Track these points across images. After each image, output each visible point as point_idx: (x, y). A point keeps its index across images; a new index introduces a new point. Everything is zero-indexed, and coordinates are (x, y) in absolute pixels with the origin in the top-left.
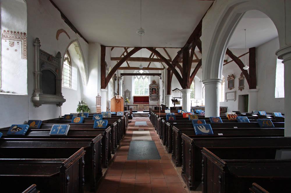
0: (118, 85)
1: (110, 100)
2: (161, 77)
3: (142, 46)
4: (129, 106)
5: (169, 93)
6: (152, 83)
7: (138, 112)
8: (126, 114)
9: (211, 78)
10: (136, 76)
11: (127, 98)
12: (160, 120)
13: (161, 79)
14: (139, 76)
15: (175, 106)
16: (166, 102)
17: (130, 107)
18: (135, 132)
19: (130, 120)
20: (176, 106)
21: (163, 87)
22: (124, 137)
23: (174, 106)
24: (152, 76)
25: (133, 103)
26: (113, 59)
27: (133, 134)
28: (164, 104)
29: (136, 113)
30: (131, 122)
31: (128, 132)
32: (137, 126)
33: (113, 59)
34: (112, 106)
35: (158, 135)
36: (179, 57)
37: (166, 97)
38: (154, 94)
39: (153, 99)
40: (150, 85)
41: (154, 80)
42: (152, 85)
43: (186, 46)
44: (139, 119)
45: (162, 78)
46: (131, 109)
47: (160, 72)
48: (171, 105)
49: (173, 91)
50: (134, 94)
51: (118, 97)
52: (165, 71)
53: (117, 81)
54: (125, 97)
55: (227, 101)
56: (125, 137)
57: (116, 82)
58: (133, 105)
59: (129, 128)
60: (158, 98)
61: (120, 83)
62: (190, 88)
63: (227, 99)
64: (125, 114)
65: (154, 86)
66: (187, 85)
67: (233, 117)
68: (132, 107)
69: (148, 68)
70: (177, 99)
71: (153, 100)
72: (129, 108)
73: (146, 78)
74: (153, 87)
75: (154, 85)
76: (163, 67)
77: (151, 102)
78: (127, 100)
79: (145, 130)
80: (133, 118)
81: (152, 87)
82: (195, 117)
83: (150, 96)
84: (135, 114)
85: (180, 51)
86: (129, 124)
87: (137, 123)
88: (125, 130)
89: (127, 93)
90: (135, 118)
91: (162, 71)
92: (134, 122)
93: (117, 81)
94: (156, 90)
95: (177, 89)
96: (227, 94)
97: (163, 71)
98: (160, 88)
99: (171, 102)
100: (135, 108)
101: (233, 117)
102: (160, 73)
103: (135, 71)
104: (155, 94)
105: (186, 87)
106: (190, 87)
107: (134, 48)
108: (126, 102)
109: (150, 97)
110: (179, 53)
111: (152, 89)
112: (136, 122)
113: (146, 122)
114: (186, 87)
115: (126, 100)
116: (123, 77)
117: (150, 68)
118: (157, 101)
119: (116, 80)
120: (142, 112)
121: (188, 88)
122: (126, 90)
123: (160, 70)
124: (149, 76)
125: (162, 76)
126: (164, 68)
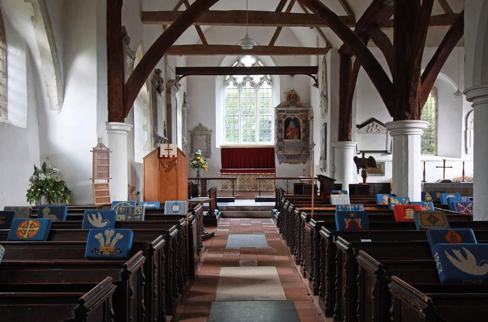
0: (169, 107)
1: (139, 159)
2: (316, 81)
4: (204, 180)
5: (344, 135)
6: (284, 100)
7: (238, 203)
8: (197, 209)
10: (228, 77)
11: (199, 152)
13: (316, 85)
14: (240, 78)
16: (333, 166)
17: (210, 185)
18: (225, 272)
19: (208, 231)
20: (371, 179)
22: (190, 285)
27: (218, 277)
28: (328, 174)
29: (230, 204)
30: (212, 236)
31: (202, 271)
33: (148, 17)
35: (306, 282)
37: (333, 149)
38: (292, 141)
40: (278, 106)
41: (292, 90)
42: (285, 106)
46: (213, 192)
47: (313, 61)
48: (353, 176)
49: (359, 127)
51: (169, 150)
52: (332, 61)
53: (163, 93)
56: (192, 289)
58: (219, 176)
59: (205, 255)
60: (306, 153)
68: (218, 185)
69: (271, 50)
71: (289, 159)
72: (204, 188)
74: (289, 116)
75: (292, 108)
76: (323, 45)
77: (282, 168)
78: (198, 160)
79: (261, 264)
80: (221, 222)
81: (285, 116)
83: (277, 145)
84: (228, 208)
86: (204, 243)
87: (235, 240)
88: (191, 264)
91: (321, 57)
92: (225, 237)
93: (163, 93)
94: (298, 125)
95: (372, 120)
97: (325, 59)
98: (312, 118)
100: (226, 187)
102: (313, 64)
103: (227, 61)
105: (407, 114)
106: (420, 114)
108: (195, 166)
109: (280, 149)
111: (284, 120)
112: (229, 236)
113: (263, 236)
114: (407, 114)
115: (195, 162)
116: (183, 81)
118: (304, 163)
119: (159, 90)
120: (250, 203)
121: (413, 118)
122: (195, 124)
123: (313, 54)
124: (277, 78)
125: (320, 75)
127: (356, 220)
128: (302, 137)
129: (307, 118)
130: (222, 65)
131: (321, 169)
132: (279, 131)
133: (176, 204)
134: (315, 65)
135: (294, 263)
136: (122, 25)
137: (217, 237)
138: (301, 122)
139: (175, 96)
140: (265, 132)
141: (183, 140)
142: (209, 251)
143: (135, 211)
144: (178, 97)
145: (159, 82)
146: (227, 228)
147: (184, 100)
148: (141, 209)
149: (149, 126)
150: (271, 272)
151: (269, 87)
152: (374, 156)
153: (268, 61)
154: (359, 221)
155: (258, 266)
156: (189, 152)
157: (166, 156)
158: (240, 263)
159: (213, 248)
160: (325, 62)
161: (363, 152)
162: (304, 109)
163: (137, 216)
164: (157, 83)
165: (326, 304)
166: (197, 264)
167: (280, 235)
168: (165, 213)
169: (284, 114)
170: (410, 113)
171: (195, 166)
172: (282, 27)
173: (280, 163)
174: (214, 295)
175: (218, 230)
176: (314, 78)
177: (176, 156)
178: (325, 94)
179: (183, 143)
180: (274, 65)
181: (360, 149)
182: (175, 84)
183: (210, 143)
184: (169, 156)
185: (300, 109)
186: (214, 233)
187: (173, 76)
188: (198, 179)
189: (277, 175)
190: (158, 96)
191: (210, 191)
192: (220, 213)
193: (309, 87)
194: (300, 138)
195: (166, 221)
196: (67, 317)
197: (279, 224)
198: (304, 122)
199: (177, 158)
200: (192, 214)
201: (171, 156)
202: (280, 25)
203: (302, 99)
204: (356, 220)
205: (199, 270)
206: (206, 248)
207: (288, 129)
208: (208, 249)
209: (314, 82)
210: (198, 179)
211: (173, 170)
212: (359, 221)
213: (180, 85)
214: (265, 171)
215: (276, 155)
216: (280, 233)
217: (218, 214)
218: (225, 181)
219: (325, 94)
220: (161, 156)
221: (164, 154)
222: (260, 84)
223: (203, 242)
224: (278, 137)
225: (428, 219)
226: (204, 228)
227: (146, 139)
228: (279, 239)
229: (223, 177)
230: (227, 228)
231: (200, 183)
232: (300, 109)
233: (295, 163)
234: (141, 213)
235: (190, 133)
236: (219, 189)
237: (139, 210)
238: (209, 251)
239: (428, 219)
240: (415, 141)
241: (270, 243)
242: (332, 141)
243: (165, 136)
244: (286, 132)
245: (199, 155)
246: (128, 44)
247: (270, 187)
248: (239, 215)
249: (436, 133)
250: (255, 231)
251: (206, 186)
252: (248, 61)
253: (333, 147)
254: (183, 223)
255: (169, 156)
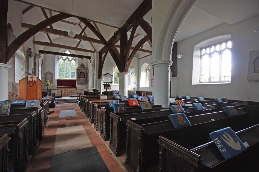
0: (35, 63)
1: (17, 81)
2: (91, 61)
3: (73, 14)
4: (50, 90)
5: (100, 76)
6: (80, 66)
7: (63, 98)
8: (45, 104)
9: (163, 59)
10: (60, 56)
11: (48, 81)
12: (87, 102)
13: (91, 62)
14: (64, 57)
15: (106, 90)
17: (52, 92)
18: (59, 131)
19: (51, 110)
20: (108, 90)
21: (93, 71)
22: (39, 145)
23: (106, 91)
24: (81, 58)
25: (57, 87)
26: (24, 25)
27: (56, 135)
29: (60, 98)
30: (53, 112)
31: (47, 133)
32: (62, 118)
33: (24, 25)
34: (22, 91)
35: (98, 133)
36: (115, 39)
37: (96, 81)
38: (82, 78)
39: (81, 83)
40: (78, 68)
41: (82, 63)
42: (80, 68)
43: (125, 25)
44: (65, 107)
45: (92, 61)
46: (54, 95)
47: (89, 54)
48: (103, 90)
49: (104, 75)
50: (57, 77)
51: (32, 78)
53: (32, 58)
54: (45, 80)
55: (151, 87)
56: (41, 147)
57: (31, 59)
58: (56, 89)
59: (49, 123)
60: (86, 82)
61: (37, 62)
62: (127, 72)
63: (152, 84)
64: (42, 105)
65: (82, 70)
66: (125, 69)
67: (182, 104)
68: (56, 92)
69: (76, 49)
70: (109, 83)
71: (81, 84)
72: (50, 93)
73: (73, 60)
74: (81, 71)
75: (82, 69)
76: (93, 50)
78: (47, 83)
79: (76, 124)
80: (57, 105)
81: (80, 71)
82: (148, 106)
83: (77, 80)
84: (60, 100)
85: (116, 32)
86: (49, 116)
87: (63, 114)
88: (40, 129)
89: (48, 75)
90: (59, 105)
91: (93, 54)
92: (58, 112)
93: (32, 58)
94: (84, 74)
95: (108, 73)
96: (152, 80)
97: (94, 54)
98: (89, 72)
99: (102, 87)
100: (59, 92)
101: (182, 104)
102: (89, 56)
103: (61, 50)
104: (83, 78)
105: (124, 71)
106: (127, 71)
107: (59, 13)
108: (46, 85)
110: (116, 34)
112: (60, 111)
113: (74, 110)
114: (124, 71)
115: (46, 84)
116: (42, 55)
117: (79, 48)
118: (86, 85)
119: (30, 56)
120: (68, 98)
121: (126, 72)
122: (47, 71)
123: (90, 52)
124: (77, 58)
126: (95, 51)
127: (122, 107)
128: (85, 77)
129: (87, 72)
130: (59, 52)
131: (92, 87)
132: (78, 75)
133: (33, 102)
134: (90, 56)
135: (90, 123)
136: (8, 22)
137: (55, 112)
138: (85, 73)
139: (38, 60)
140: (73, 76)
141: (41, 76)
142: (51, 120)
143: (3, 108)
144: (40, 60)
145: (30, 53)
146: (59, 108)
147: (42, 63)
148: (7, 107)
149: (24, 69)
150: (80, 129)
151: (75, 62)
152: (109, 83)
153: (74, 52)
154: (123, 108)
155: (75, 126)
156: (44, 80)
157: (31, 80)
158: (66, 125)
159: (53, 118)
160: (94, 55)
161: (106, 83)
162: (86, 69)
163: (4, 110)
164: (29, 53)
165: (117, 150)
166: (44, 129)
167: (81, 110)
168: (26, 107)
169: (80, 70)
170: (125, 70)
171: (46, 85)
172: (81, 41)
173: (78, 85)
174: (53, 149)
175: (55, 109)
176: (90, 60)
177: (36, 81)
178: (94, 64)
179: (41, 77)
180: (76, 54)
181: (104, 82)
182: (38, 55)
183: (53, 78)
184: (32, 81)
185: (85, 69)
186: (53, 111)
187: (38, 53)
188: (48, 90)
189: (77, 89)
190: (30, 58)
191: (52, 95)
192: (56, 102)
193: (88, 63)
194: (84, 78)
195: (22, 114)
196: (132, 24)
197: (80, 105)
198: (86, 73)
199: (36, 81)
200: (42, 107)
201: (33, 81)
202: (81, 40)
203: (86, 66)
204: (122, 107)
205: (45, 132)
206: (49, 118)
207: (81, 75)
208: (51, 119)
209: (90, 61)
210: (48, 90)
211: (35, 86)
212: (123, 108)
213: (40, 56)
214: (73, 88)
215: (77, 83)
216: (81, 108)
217: (55, 102)
218: (58, 91)
219: (94, 64)
220: (28, 80)
221: (30, 79)
222: (72, 60)
223: (48, 116)
224: (77, 77)
225: (145, 105)
226: (49, 109)
227: (23, 74)
228: (81, 111)
229: (58, 89)
230: (59, 108)
231: (48, 91)
232: (85, 69)
233: (83, 85)
234: (7, 109)
235: (44, 74)
236: (56, 93)
237: (6, 107)
238: (51, 120)
239: (145, 105)
240: (126, 79)
241: (78, 114)
242: (96, 79)
243: (33, 74)
244: (80, 76)
245: (48, 82)
246: (12, 31)
247: (75, 92)
248: (65, 102)
249: (45, 90)
250: (71, 109)
251: (50, 93)
252: (67, 52)
253: (97, 81)
254: (34, 114)
255: (32, 81)
